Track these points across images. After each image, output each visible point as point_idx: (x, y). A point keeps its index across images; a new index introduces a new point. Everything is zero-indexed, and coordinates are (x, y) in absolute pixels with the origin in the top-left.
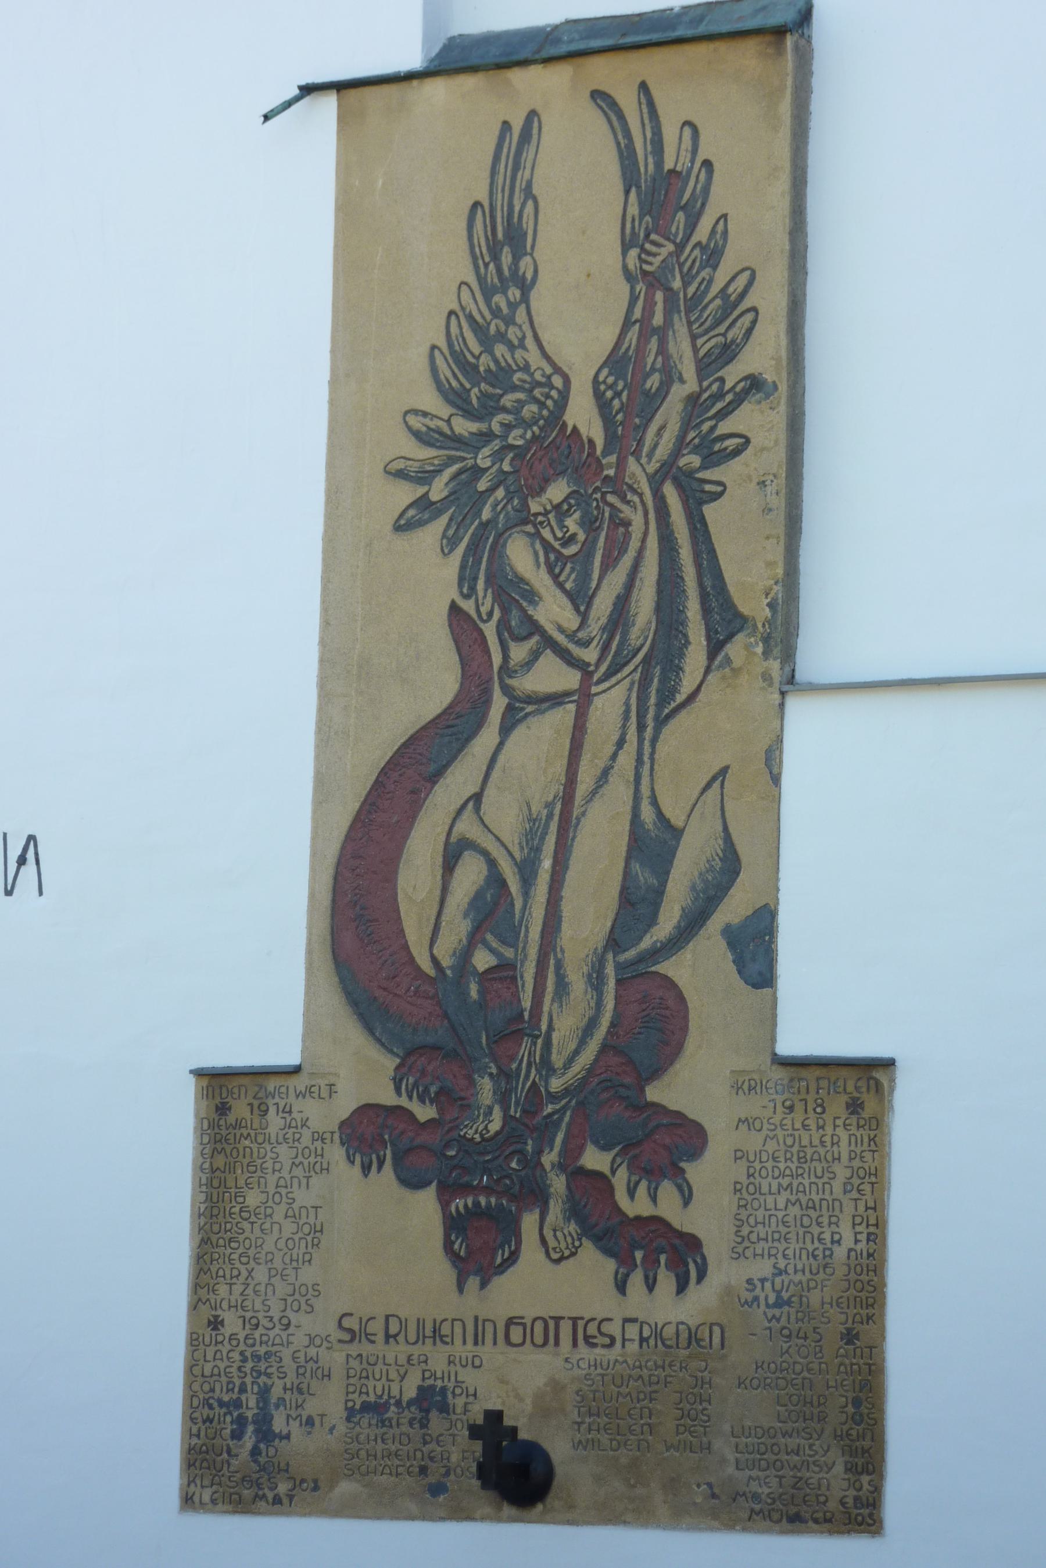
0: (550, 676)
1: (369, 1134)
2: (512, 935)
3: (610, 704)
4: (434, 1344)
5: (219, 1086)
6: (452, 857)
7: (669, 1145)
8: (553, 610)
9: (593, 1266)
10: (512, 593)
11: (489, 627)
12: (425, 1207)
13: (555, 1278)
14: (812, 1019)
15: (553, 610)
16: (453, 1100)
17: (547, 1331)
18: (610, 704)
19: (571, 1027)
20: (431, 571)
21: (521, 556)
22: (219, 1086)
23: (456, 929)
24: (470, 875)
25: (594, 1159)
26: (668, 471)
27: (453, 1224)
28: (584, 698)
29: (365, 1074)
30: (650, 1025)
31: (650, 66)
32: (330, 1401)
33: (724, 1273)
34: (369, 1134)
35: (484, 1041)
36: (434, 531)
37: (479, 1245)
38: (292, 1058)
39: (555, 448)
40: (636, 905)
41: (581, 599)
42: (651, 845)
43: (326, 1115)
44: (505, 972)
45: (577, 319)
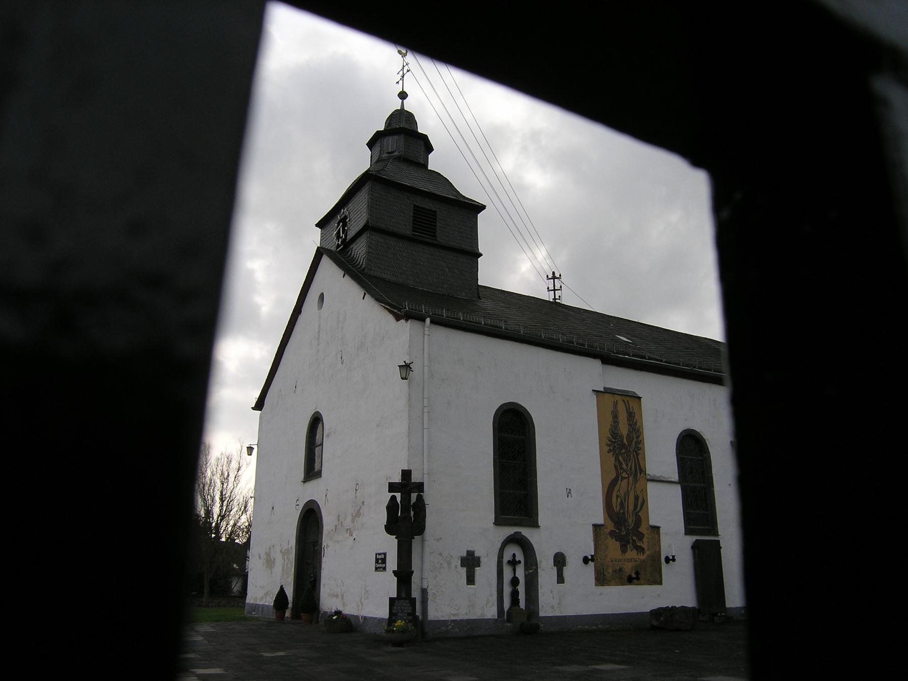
0: (624, 475)
1: (612, 534)
2: (624, 508)
3: (631, 479)
4: (554, 273)
5: (390, 599)
6: (617, 496)
7: (641, 536)
8: (624, 466)
9: (635, 552)
10: (620, 463)
11: (618, 467)
12: (618, 543)
13: (632, 554)
14: (652, 523)
15: (624, 466)
16: (620, 530)
17: (630, 560)
18: (631, 479)
19: (631, 521)
20: (611, 459)
21: (621, 459)
22: (390, 599)
23: (619, 507)
24: (619, 500)
25: (634, 538)
26: (634, 450)
27: (621, 546)
28: (628, 478)
29: (611, 527)
30: (638, 522)
31: (628, 398)
32: (610, 570)
33: (647, 553)
34: (612, 534)
35: (412, 513)
36: (611, 454)
37: (624, 550)
38: (603, 522)
39: (622, 446)
40: (636, 506)
41: (627, 465)
42: (637, 498)
43: (607, 531)
44: (624, 513)
45: (624, 429)
